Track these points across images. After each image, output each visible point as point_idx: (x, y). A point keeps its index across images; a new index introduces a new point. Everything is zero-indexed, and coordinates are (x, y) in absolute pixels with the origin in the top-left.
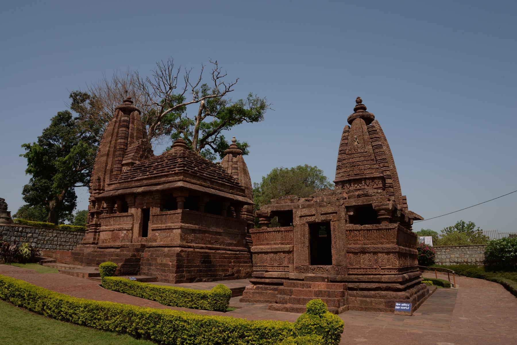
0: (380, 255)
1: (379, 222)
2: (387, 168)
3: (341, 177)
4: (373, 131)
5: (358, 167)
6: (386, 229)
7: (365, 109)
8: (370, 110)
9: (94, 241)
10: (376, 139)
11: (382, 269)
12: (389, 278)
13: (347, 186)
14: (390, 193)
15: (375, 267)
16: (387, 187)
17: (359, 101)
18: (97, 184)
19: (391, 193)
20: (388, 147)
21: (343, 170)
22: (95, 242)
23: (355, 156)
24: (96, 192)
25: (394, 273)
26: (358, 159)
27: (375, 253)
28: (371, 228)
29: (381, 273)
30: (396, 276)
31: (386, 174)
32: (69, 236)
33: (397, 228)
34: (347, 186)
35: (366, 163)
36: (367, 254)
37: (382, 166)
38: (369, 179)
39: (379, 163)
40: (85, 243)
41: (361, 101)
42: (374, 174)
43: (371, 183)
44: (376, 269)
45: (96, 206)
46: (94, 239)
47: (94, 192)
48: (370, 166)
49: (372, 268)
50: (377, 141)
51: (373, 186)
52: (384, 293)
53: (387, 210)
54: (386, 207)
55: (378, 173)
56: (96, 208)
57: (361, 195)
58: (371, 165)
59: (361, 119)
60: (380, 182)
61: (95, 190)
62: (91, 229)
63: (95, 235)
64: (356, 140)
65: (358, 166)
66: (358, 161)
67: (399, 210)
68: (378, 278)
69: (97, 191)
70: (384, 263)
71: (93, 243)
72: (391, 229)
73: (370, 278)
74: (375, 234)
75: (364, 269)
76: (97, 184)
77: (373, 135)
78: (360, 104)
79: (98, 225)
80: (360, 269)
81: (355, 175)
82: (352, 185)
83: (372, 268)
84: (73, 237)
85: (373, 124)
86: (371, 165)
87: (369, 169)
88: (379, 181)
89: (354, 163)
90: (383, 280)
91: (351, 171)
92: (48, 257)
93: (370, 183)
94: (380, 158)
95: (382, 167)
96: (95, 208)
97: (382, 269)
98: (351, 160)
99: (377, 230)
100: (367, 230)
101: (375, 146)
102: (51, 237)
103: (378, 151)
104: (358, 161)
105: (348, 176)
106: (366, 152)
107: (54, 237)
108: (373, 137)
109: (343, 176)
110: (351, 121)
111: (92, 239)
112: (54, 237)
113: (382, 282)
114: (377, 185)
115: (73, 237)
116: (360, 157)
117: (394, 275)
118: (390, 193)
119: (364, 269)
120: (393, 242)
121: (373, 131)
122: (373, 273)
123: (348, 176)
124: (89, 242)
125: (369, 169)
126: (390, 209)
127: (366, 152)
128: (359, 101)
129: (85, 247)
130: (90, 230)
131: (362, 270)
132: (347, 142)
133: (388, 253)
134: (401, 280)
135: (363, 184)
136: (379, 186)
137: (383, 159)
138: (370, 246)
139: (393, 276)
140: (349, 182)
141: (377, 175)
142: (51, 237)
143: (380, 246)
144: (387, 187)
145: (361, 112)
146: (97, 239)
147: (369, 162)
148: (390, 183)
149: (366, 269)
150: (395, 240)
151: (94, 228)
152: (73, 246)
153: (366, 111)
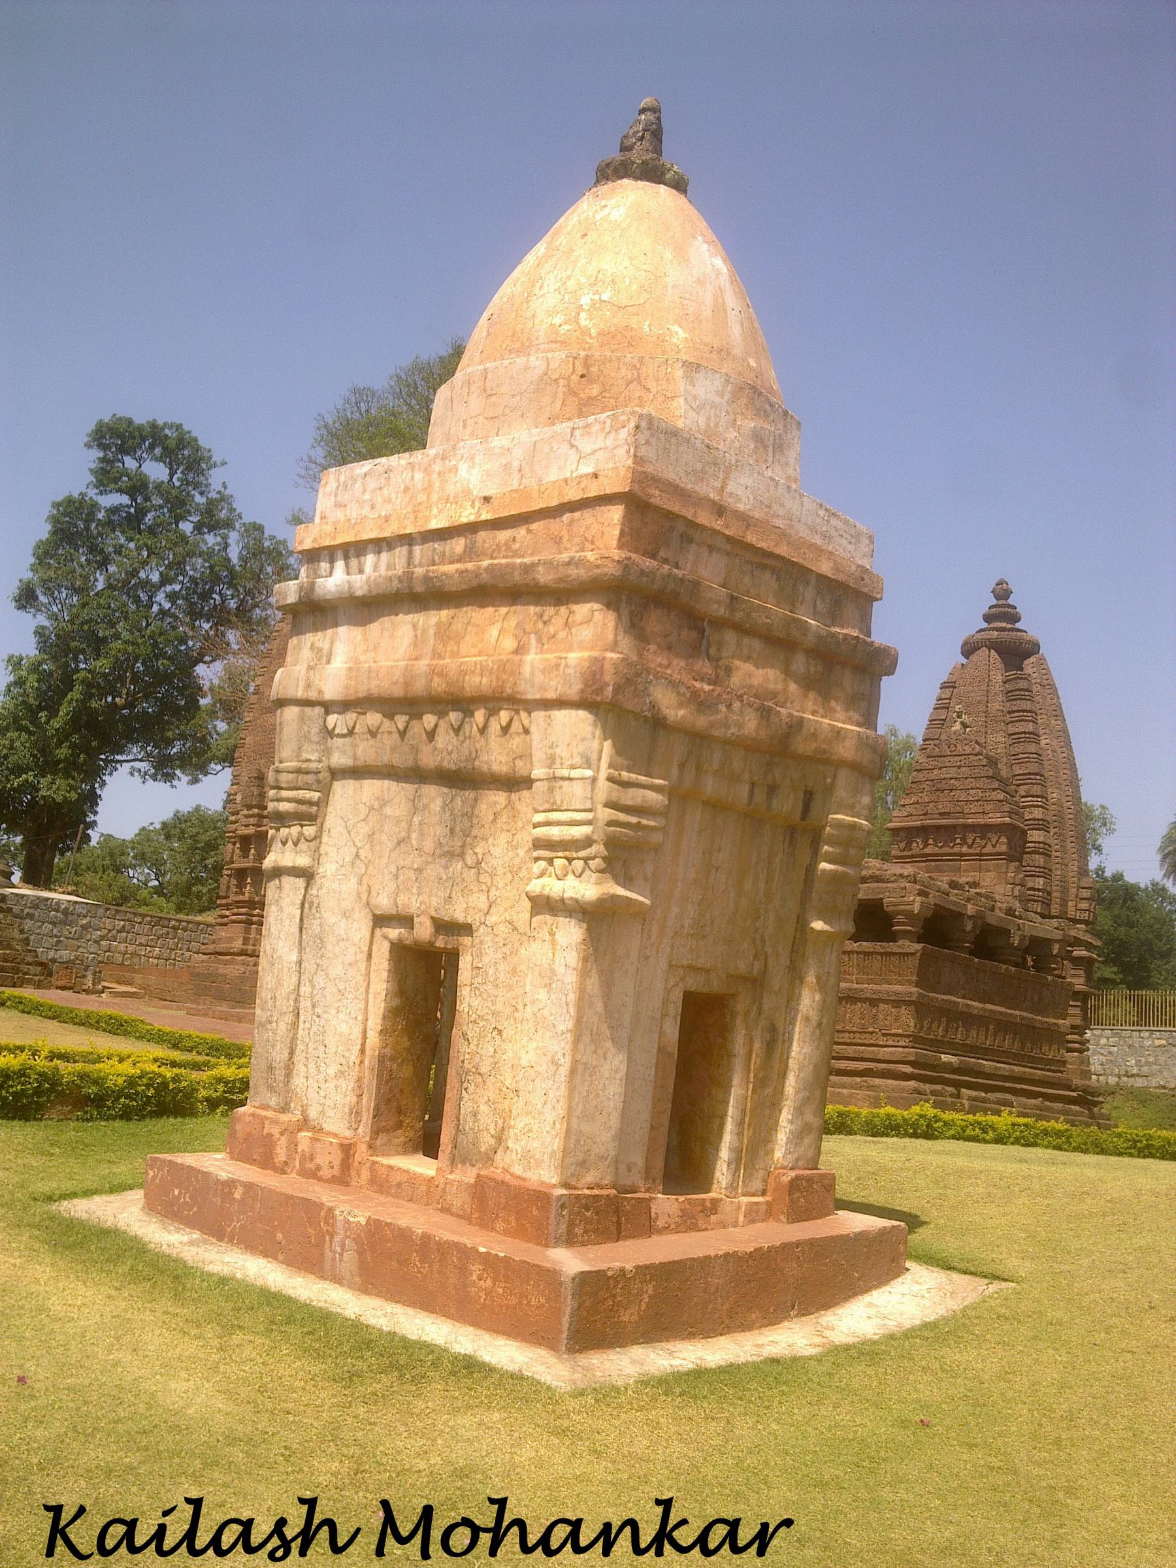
0: (882, 1006)
1: (892, 937)
2: (1035, 799)
3: (907, 816)
4: (1016, 690)
5: (952, 794)
6: (900, 954)
7: (1015, 618)
8: (1031, 626)
9: (244, 947)
10: (1021, 714)
11: (883, 1035)
12: (892, 1053)
13: (917, 843)
14: (1034, 869)
15: (871, 1030)
16: (1028, 853)
17: (1002, 592)
18: (256, 791)
19: (1038, 870)
20: (1064, 736)
21: (914, 799)
22: (247, 950)
23: (949, 764)
24: (251, 812)
25: (904, 1044)
26: (953, 772)
27: (873, 1003)
28: (871, 950)
29: (881, 1043)
30: (906, 1050)
31: (1031, 817)
32: (156, 930)
33: (918, 954)
34: (917, 843)
35: (973, 785)
36: (859, 1004)
37: (1023, 793)
38: (973, 828)
39: (1018, 785)
40: (218, 950)
41: (1007, 594)
42: (990, 815)
43: (978, 840)
44: (872, 1033)
45: (252, 851)
46: (246, 941)
47: (245, 812)
48: (980, 794)
49: (865, 1033)
50: (1023, 720)
51: (984, 847)
52: (877, 1081)
53: (909, 915)
54: (908, 907)
55: (998, 815)
56: (251, 857)
57: (868, 879)
58: (984, 790)
59: (992, 651)
60: (1004, 839)
61: (249, 807)
62: (234, 915)
63: (247, 931)
64: (959, 717)
65: (951, 790)
66: (951, 779)
67: (970, 917)
68: (873, 1052)
69: (256, 811)
70: (887, 1023)
71: (243, 953)
72: (907, 954)
73: (859, 1051)
74: (877, 962)
75: (850, 1032)
76: (256, 791)
77: (1014, 702)
78: (1003, 602)
79: (255, 903)
80: (843, 1032)
81: (940, 814)
82: (931, 841)
83: (865, 1033)
84: (168, 933)
85: (1029, 665)
86: (984, 790)
87: (977, 801)
88: (1000, 837)
89: (944, 782)
90: (880, 1057)
91: (931, 805)
92: (119, 983)
93: (974, 840)
94: (1021, 772)
95: (1023, 797)
96: (247, 857)
97: (883, 1035)
98: (935, 772)
99: (881, 954)
100: (865, 953)
101: (1016, 736)
102: (109, 931)
103: (1020, 751)
104: (951, 779)
105: (924, 815)
106: (976, 755)
107: (118, 932)
108: (1014, 708)
109: (911, 815)
110: (968, 650)
111: (241, 941)
112: (118, 932)
113: (879, 1061)
114: (994, 846)
115: (168, 933)
116: (959, 767)
117: (904, 1047)
118: (1034, 869)
119: (850, 1032)
120: (909, 982)
121: (1016, 690)
122: (866, 1042)
123: (924, 815)
124: (230, 948)
125: (977, 801)
126: (916, 912)
127: (976, 755)
128: (1002, 592)
129: (220, 962)
130: (234, 917)
131: (846, 1035)
132: (944, 717)
133: (897, 1003)
134: (913, 1058)
135: (958, 841)
136: (998, 849)
137: (1029, 774)
138: (866, 985)
139: (901, 1049)
140: (924, 831)
141: (996, 819)
142: (109, 931)
143: (885, 987)
144: (1028, 853)
145: (997, 629)
146: (251, 942)
147: (980, 783)
148: (1039, 843)
149: (854, 1032)
150: (915, 978)
151: (244, 910)
152: (166, 960)
153: (1018, 625)
